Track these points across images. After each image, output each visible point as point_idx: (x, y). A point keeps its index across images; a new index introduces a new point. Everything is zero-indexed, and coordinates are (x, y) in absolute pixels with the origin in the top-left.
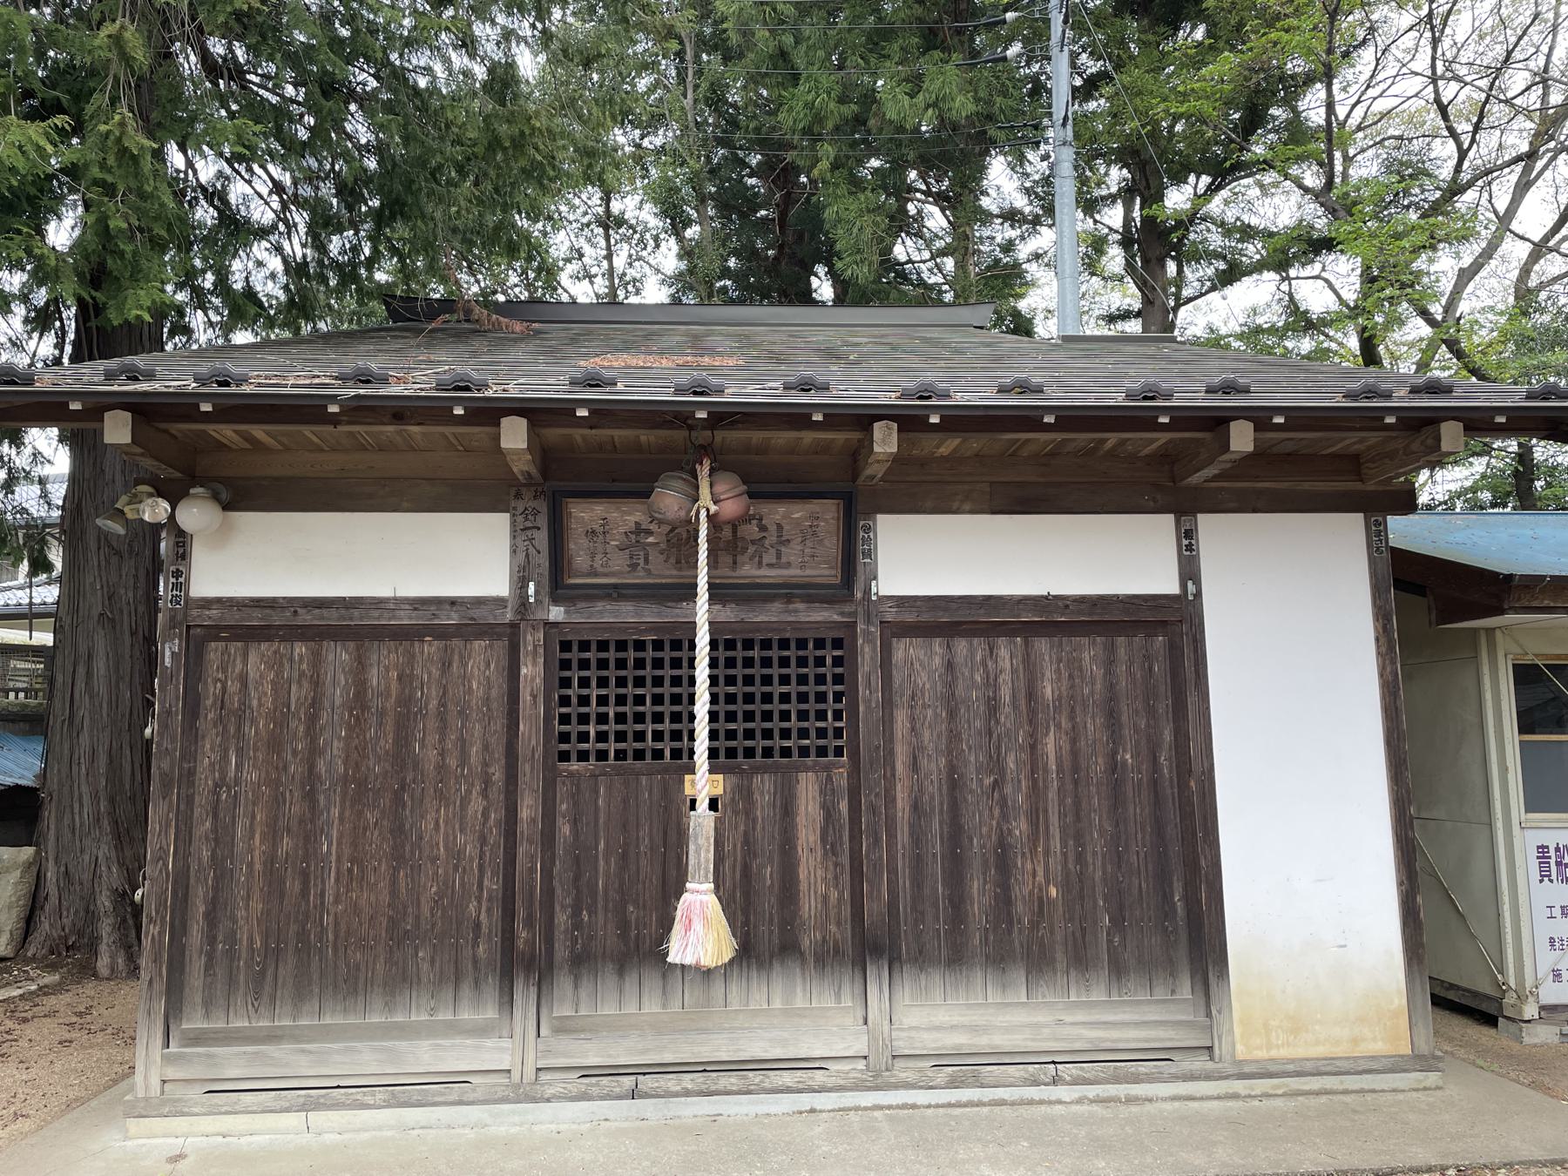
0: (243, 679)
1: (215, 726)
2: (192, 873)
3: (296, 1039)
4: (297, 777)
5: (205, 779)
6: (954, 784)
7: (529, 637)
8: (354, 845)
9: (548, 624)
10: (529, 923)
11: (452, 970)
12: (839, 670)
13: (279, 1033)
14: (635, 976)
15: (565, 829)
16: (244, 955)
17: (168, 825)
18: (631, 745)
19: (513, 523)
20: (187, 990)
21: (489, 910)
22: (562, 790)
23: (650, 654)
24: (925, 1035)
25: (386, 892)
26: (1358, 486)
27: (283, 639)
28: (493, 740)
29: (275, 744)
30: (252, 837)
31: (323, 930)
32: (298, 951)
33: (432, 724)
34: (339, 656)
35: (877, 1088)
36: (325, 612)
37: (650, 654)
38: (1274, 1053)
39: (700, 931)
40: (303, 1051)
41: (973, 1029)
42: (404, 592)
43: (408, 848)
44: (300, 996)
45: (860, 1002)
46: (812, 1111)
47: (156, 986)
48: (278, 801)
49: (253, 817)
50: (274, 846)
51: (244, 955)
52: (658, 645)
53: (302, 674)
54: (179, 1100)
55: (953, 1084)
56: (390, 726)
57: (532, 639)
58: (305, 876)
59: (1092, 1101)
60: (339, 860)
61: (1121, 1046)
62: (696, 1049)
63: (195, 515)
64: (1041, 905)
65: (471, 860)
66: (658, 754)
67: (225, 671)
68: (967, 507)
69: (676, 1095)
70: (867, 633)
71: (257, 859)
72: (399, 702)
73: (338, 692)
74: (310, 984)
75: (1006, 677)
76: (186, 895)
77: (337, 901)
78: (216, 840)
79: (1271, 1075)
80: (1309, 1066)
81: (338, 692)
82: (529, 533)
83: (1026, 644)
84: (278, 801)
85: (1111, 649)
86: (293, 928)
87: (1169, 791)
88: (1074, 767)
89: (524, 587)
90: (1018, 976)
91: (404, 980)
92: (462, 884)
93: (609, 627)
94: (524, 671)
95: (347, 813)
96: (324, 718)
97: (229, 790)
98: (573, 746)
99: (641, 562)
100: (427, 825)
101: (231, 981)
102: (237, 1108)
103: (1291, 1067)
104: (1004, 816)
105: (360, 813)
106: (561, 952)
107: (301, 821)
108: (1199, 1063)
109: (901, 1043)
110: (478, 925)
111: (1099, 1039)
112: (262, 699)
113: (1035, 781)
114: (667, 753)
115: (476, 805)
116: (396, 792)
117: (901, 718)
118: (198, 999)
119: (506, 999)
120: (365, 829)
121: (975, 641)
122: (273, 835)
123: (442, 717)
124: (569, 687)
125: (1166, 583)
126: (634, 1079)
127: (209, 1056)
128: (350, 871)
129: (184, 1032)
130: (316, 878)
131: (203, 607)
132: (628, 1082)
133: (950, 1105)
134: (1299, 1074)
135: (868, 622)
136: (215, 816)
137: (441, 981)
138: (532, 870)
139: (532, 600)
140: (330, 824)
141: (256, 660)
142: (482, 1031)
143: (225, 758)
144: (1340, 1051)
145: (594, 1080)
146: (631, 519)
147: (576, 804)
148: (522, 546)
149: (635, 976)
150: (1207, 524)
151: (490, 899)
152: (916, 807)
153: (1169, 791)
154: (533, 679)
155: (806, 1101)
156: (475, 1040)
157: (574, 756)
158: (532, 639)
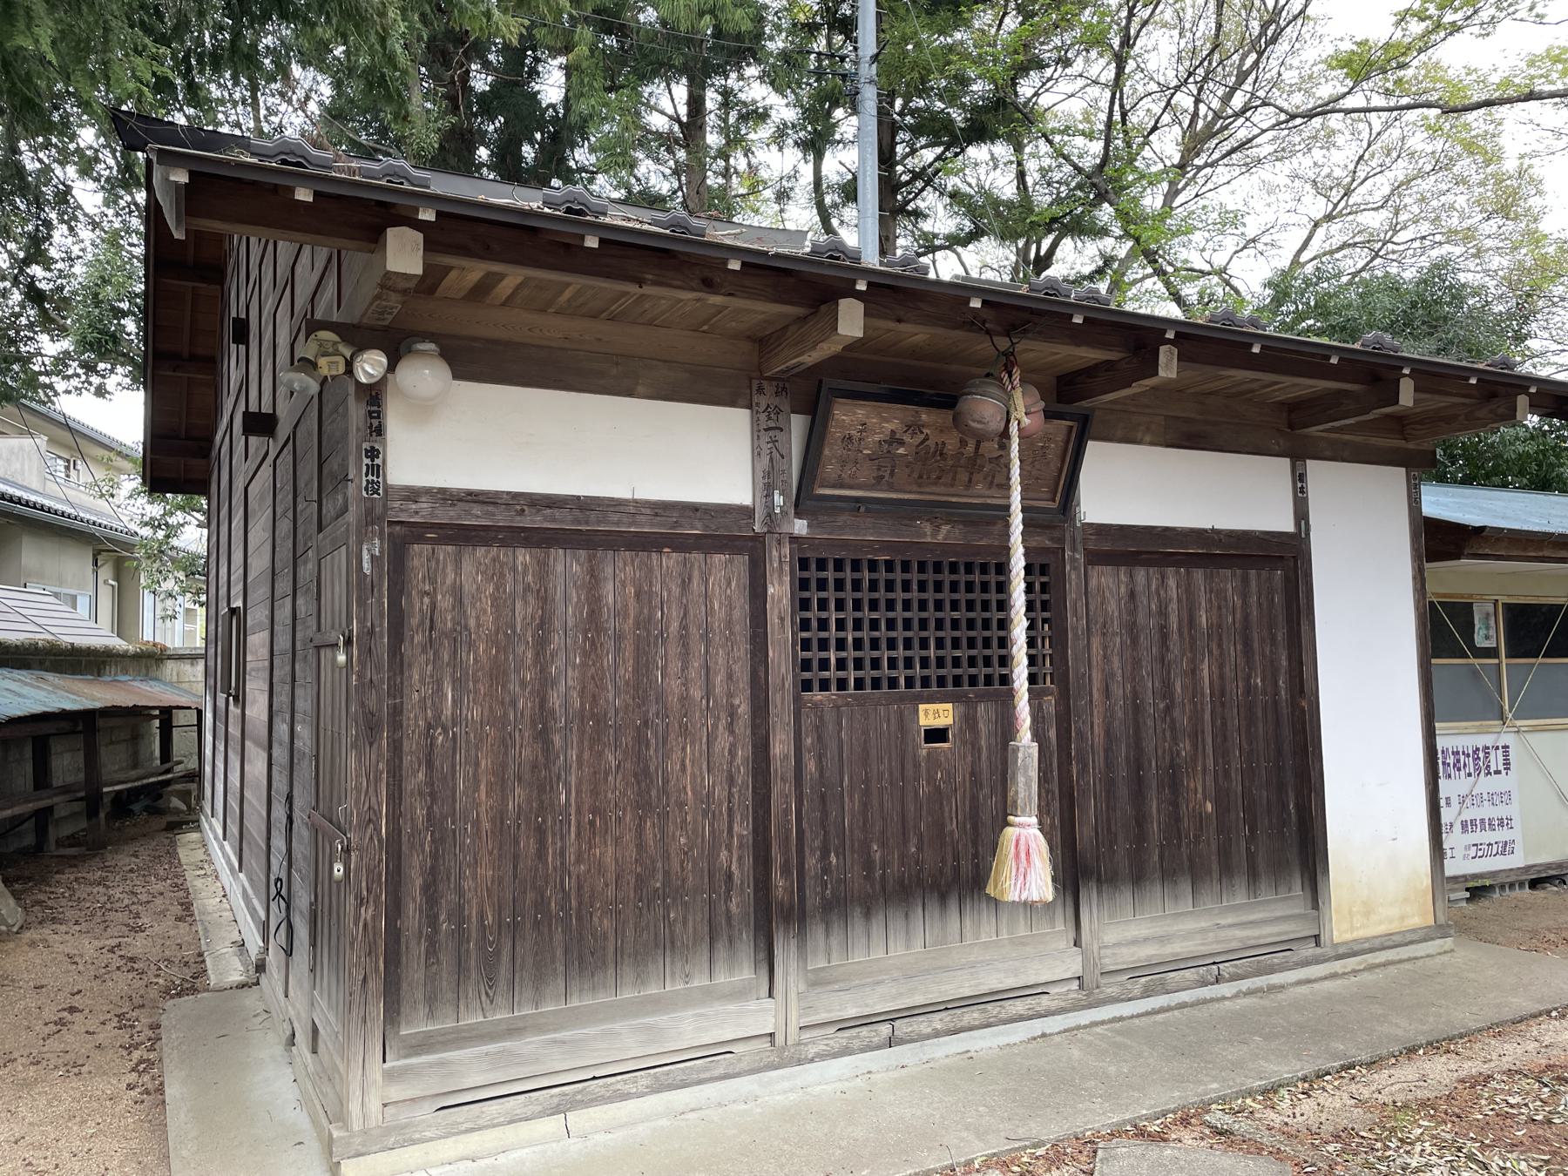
0: (457, 592)
1: (424, 651)
2: (404, 839)
3: (540, 1029)
4: (527, 713)
5: (414, 720)
6: (1136, 709)
7: (775, 553)
8: (595, 793)
9: (794, 539)
10: (786, 871)
11: (706, 929)
12: (1046, 597)
13: (521, 1025)
14: (881, 917)
15: (811, 766)
16: (474, 935)
17: (378, 780)
18: (868, 673)
19: (755, 422)
20: (404, 986)
21: (740, 858)
22: (808, 722)
23: (882, 575)
24: (1124, 950)
25: (632, 846)
26: (1401, 444)
27: (504, 544)
28: (736, 668)
29: (498, 674)
30: (477, 789)
31: (566, 896)
32: (537, 923)
33: (674, 649)
34: (567, 566)
35: (1090, 1006)
36: (557, 513)
37: (882, 575)
38: (1355, 935)
39: (1026, 862)
40: (555, 1041)
41: (1162, 940)
42: (642, 495)
43: (654, 793)
44: (539, 981)
45: (1071, 924)
46: (1044, 1035)
47: (371, 984)
48: (505, 743)
49: (477, 764)
50: (504, 799)
51: (474, 935)
52: (889, 566)
53: (527, 588)
54: (406, 1126)
55: (1147, 993)
56: (628, 647)
57: (779, 559)
58: (540, 832)
59: (1245, 994)
60: (579, 811)
61: (1262, 941)
62: (943, 988)
63: (424, 376)
64: (1200, 818)
65: (720, 805)
66: (893, 683)
67: (433, 582)
68: (1148, 438)
69: (928, 1037)
70: (1073, 560)
71: (483, 817)
72: (637, 625)
73: (569, 610)
74: (553, 962)
75: (1174, 606)
76: (398, 868)
77: (578, 861)
78: (432, 795)
79: (1354, 954)
80: (1377, 943)
81: (569, 610)
82: (771, 433)
83: (1188, 573)
84: (505, 743)
85: (1245, 580)
86: (530, 896)
87: (1285, 711)
88: (1220, 693)
89: (769, 496)
90: (1185, 887)
91: (657, 946)
92: (712, 832)
93: (845, 544)
94: (771, 590)
95: (586, 755)
96: (557, 641)
97: (445, 730)
98: (814, 675)
99: (887, 475)
100: (673, 766)
101: (461, 968)
102: (481, 1122)
103: (1367, 945)
104: (1175, 740)
105: (600, 754)
106: (813, 900)
107: (534, 767)
108: (1309, 950)
109: (1107, 961)
110: (730, 876)
111: (1249, 938)
112: (481, 616)
113: (1195, 704)
114: (902, 681)
115: (723, 741)
116: (638, 728)
117: (1096, 642)
118: (419, 995)
119: (762, 955)
120: (607, 774)
121: (1151, 570)
122: (500, 784)
123: (684, 639)
124: (871, 609)
125: (1284, 522)
126: (891, 1027)
127: (442, 1064)
128: (592, 823)
129: (403, 1039)
130: (554, 835)
131: (407, 499)
132: (885, 1029)
133: (1147, 1014)
134: (1371, 950)
135: (1074, 550)
136: (430, 765)
137: (694, 944)
138: (787, 812)
139: (777, 511)
140: (567, 769)
141: (470, 571)
142: (738, 994)
143: (439, 690)
144: (1394, 927)
145: (854, 1032)
146: (889, 426)
147: (820, 738)
148: (766, 447)
149: (881, 917)
150: (1311, 464)
151: (741, 846)
152: (1108, 733)
153: (1285, 711)
154: (780, 600)
155: (1037, 1026)
156: (716, 1006)
157: (816, 685)
158: (779, 559)
